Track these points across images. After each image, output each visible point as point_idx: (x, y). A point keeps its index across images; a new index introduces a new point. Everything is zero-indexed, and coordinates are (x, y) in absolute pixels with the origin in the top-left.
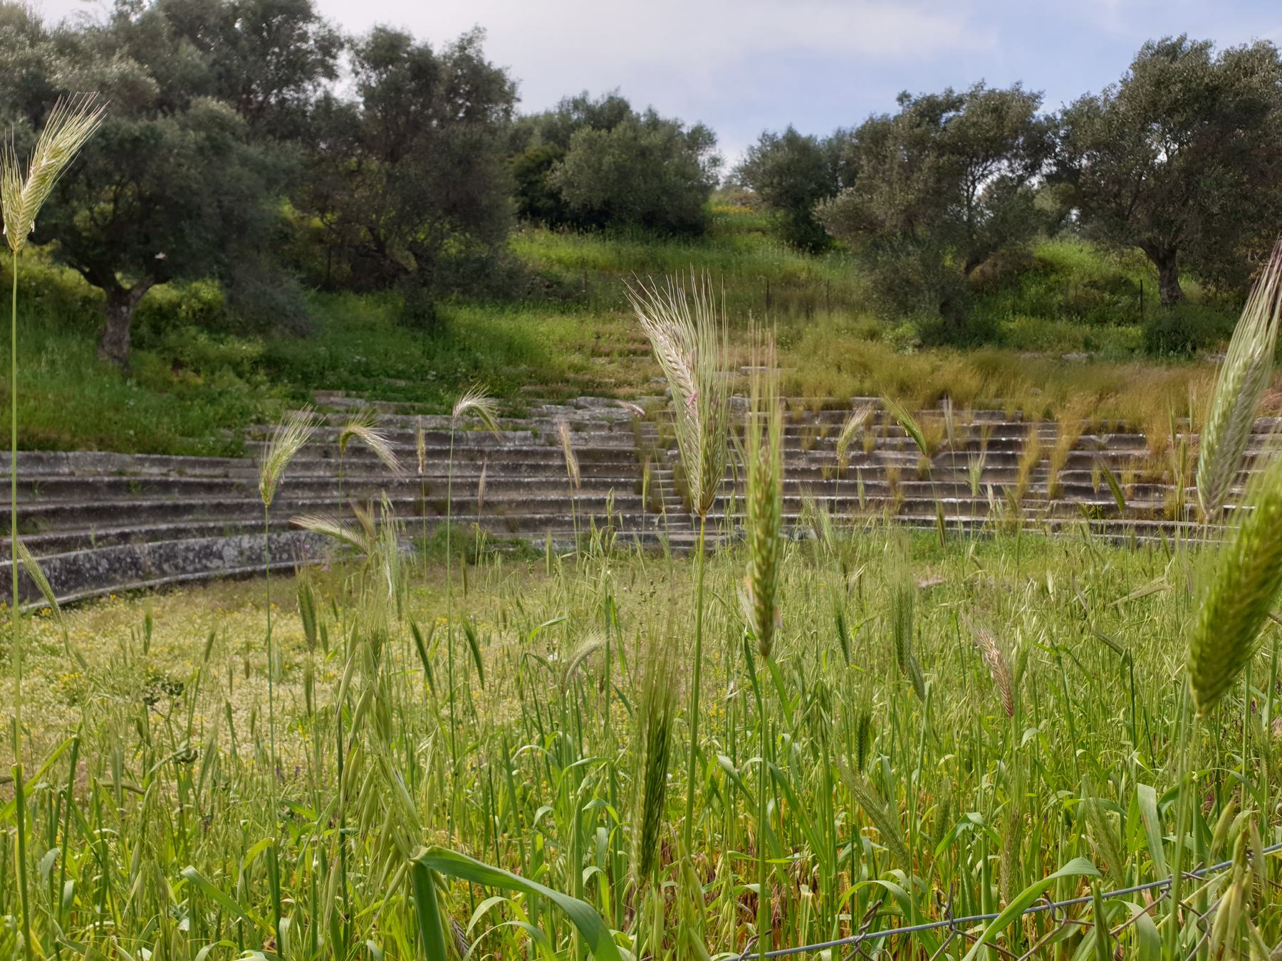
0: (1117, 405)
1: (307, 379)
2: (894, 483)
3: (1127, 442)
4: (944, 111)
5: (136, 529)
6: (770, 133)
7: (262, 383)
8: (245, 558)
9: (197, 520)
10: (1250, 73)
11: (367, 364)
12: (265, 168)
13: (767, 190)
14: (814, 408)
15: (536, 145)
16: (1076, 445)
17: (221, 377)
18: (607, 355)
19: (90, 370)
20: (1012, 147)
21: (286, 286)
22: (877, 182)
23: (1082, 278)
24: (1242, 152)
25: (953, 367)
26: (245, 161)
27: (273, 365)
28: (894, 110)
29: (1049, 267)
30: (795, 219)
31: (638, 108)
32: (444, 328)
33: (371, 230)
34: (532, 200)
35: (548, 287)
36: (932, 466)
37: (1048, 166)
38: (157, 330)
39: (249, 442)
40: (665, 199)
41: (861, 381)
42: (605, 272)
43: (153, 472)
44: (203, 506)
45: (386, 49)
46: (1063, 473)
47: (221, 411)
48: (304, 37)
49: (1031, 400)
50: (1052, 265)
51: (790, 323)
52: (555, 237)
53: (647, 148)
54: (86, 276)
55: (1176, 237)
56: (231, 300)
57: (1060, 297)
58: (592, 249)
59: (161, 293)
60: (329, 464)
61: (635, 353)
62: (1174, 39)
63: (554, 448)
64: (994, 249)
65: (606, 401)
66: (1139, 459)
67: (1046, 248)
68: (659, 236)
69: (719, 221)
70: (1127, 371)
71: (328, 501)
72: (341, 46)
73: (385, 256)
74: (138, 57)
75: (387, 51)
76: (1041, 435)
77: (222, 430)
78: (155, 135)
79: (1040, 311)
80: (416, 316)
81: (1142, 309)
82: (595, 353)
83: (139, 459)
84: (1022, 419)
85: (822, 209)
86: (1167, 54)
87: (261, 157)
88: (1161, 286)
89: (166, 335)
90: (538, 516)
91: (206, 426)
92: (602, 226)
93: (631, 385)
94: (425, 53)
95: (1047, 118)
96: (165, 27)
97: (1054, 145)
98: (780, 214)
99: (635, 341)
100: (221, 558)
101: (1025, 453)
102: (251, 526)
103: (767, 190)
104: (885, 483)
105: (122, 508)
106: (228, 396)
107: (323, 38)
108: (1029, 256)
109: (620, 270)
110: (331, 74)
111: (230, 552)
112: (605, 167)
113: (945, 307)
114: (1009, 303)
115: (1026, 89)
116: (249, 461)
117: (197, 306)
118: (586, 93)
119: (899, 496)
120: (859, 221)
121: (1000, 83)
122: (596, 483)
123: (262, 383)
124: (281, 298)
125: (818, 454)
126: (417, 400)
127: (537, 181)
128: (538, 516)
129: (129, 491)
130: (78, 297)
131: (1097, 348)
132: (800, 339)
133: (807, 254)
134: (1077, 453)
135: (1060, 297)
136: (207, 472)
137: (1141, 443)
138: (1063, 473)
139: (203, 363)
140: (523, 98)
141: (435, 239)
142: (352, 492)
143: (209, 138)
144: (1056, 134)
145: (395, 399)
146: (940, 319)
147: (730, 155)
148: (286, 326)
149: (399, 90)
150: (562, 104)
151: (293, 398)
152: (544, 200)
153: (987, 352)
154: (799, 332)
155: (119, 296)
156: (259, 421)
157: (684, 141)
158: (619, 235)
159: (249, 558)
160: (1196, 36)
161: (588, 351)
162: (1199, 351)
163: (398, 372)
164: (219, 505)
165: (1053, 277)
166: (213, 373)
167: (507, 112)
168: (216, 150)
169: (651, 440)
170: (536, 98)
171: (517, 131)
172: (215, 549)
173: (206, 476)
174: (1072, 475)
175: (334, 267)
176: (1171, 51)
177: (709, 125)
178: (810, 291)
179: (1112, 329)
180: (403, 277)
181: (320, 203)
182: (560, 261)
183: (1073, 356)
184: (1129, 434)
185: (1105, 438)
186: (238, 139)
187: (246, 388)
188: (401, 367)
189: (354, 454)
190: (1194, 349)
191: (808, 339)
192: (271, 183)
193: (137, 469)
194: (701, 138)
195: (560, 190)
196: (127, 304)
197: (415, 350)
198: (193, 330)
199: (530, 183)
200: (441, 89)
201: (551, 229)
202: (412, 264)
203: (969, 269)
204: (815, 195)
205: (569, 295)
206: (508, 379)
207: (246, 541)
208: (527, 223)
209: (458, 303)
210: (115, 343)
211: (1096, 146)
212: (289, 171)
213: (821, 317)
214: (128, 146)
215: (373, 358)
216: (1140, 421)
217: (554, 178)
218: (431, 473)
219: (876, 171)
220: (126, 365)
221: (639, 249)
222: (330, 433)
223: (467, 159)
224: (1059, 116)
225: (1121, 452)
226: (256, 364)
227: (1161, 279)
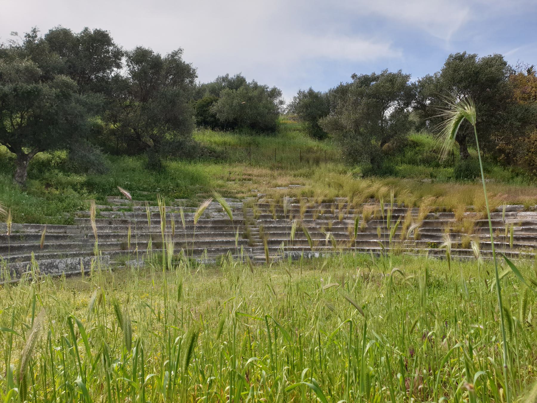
0: (443, 201)
1: (104, 191)
2: (351, 233)
3: (447, 216)
4: (371, 81)
5: (20, 256)
6: (302, 91)
7: (85, 193)
8: (68, 268)
9: (50, 252)
10: (491, 66)
11: (131, 185)
12: (87, 104)
13: (301, 114)
14: (319, 202)
15: (207, 96)
16: (427, 217)
17: (67, 191)
18: (234, 180)
19: (7, 188)
20: (398, 96)
21: (94, 152)
22: (344, 109)
23: (429, 149)
24: (490, 98)
25: (378, 186)
26: (78, 101)
27: (90, 186)
28: (351, 81)
29: (415, 144)
30: (312, 126)
31: (249, 81)
32: (165, 170)
33: (135, 130)
34: (205, 117)
35: (210, 153)
36: (367, 226)
37: (414, 104)
38: (41, 171)
39: (76, 218)
40: (259, 117)
41: (339, 191)
42: (234, 147)
43: (31, 231)
44: (53, 245)
45: (141, 56)
46: (420, 229)
47: (65, 205)
48: (108, 52)
49: (407, 198)
50: (417, 143)
51: (310, 168)
52: (214, 133)
53: (251, 97)
54: (10, 149)
55: (465, 132)
56: (71, 159)
57: (420, 156)
58: (229, 138)
59: (42, 156)
60: (111, 227)
61: (245, 180)
62: (461, 54)
63: (209, 219)
64: (392, 137)
65: (232, 199)
66: (452, 223)
67: (413, 136)
68: (257, 132)
69: (282, 127)
70: (446, 186)
71: (109, 243)
72: (123, 55)
73: (140, 140)
74: (34, 59)
75: (141, 57)
76: (411, 213)
77: (65, 213)
78: (39, 91)
79: (412, 162)
80: (153, 165)
81: (453, 161)
82: (228, 180)
83: (26, 226)
84: (404, 207)
85: (321, 122)
86: (459, 59)
87: (85, 99)
88: (461, 152)
89: (44, 173)
90: (200, 249)
91: (58, 211)
92: (233, 129)
93: (243, 193)
94: (158, 57)
95: (412, 84)
96: (47, 46)
97: (416, 95)
98: (307, 123)
99: (245, 175)
100: (57, 268)
101: (405, 221)
102: (74, 254)
103: (301, 114)
104: (347, 233)
105: (15, 247)
106: (68, 199)
107: (115, 52)
108: (406, 140)
109: (240, 146)
110: (119, 66)
111: (62, 266)
112: (234, 104)
113: (372, 161)
114: (399, 159)
115: (404, 73)
116: (76, 226)
117: (59, 161)
118: (228, 75)
119: (354, 239)
120: (337, 126)
121: (393, 70)
122: (226, 234)
123: (85, 193)
124: (93, 158)
125: (320, 221)
126: (151, 200)
127: (207, 110)
128: (200, 249)
129: (19, 240)
130: (7, 157)
131: (435, 177)
132: (314, 174)
133: (317, 140)
134: (427, 220)
135: (420, 156)
136: (57, 231)
137: (453, 216)
138: (420, 229)
139: (59, 185)
140: (199, 76)
141: (161, 133)
142: (120, 239)
143: (61, 91)
144: (416, 91)
145: (142, 200)
146: (371, 166)
147: (288, 98)
148: (94, 169)
149: (145, 73)
150: (218, 79)
151: (98, 199)
152: (209, 118)
153: (391, 179)
154: (313, 171)
155: (23, 157)
156: (81, 209)
157: (269, 94)
158: (241, 132)
159: (71, 268)
160: (470, 52)
161: (225, 179)
162: (477, 178)
163: (144, 188)
164: (60, 245)
165: (417, 148)
166: (63, 189)
167: (191, 82)
168: (64, 96)
169: (251, 215)
170: (204, 78)
171: (199, 90)
172: (55, 264)
173: (56, 233)
174: (424, 229)
175: (120, 145)
176: (460, 58)
177: (278, 87)
178: (318, 155)
179: (442, 169)
180: (148, 149)
181: (114, 118)
182: (215, 143)
183: (425, 180)
184: (448, 212)
185: (438, 214)
186: (75, 92)
187: (77, 195)
188: (145, 186)
189: (122, 223)
190: (475, 177)
191: (317, 174)
192: (89, 110)
193: (25, 230)
194: (275, 93)
195: (216, 114)
196: (26, 160)
197: (152, 179)
198: (56, 171)
199: (204, 111)
200: (163, 73)
201: (212, 130)
202: (151, 142)
203: (382, 145)
204: (321, 116)
205: (219, 156)
206: (191, 191)
207: (69, 261)
208: (202, 127)
209: (171, 160)
210: (20, 177)
211: (431, 95)
212: (98, 105)
213: (322, 165)
214: (26, 95)
215: (133, 183)
216: (453, 207)
217: (213, 109)
218: (155, 231)
219: (344, 106)
220: (25, 186)
221: (249, 138)
222: (113, 214)
223: (173, 101)
224: (417, 83)
225: (444, 220)
226: (83, 185)
227: (461, 149)
